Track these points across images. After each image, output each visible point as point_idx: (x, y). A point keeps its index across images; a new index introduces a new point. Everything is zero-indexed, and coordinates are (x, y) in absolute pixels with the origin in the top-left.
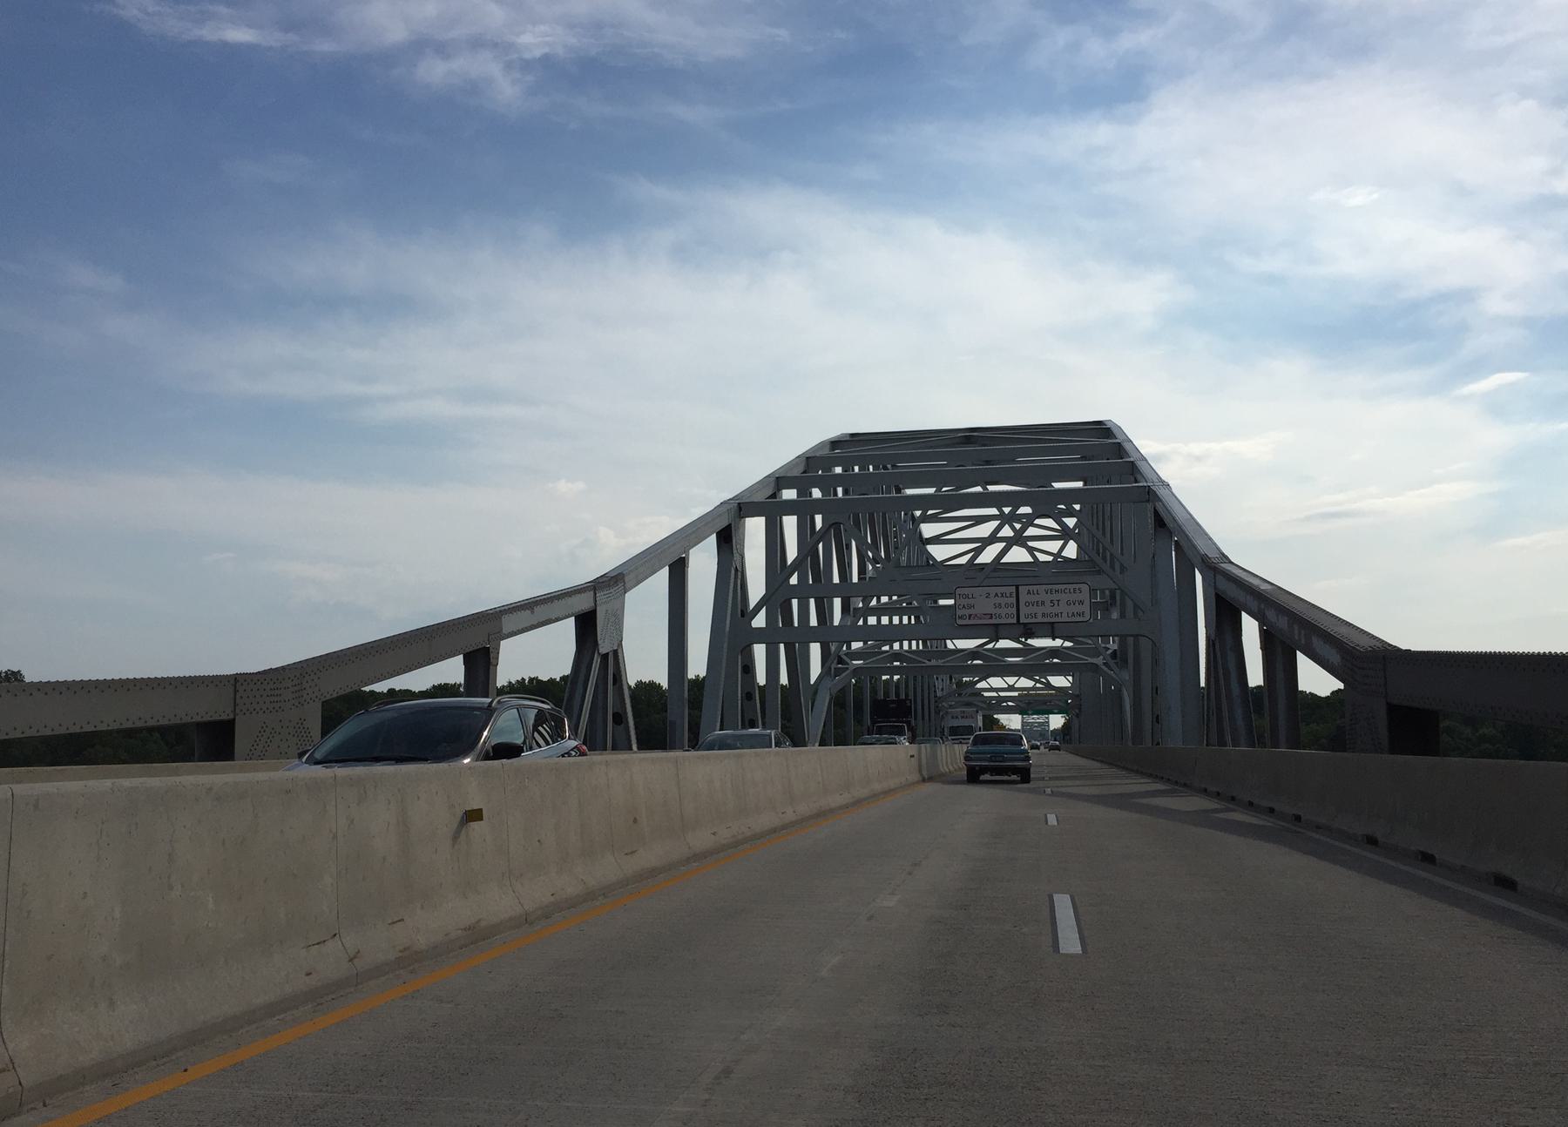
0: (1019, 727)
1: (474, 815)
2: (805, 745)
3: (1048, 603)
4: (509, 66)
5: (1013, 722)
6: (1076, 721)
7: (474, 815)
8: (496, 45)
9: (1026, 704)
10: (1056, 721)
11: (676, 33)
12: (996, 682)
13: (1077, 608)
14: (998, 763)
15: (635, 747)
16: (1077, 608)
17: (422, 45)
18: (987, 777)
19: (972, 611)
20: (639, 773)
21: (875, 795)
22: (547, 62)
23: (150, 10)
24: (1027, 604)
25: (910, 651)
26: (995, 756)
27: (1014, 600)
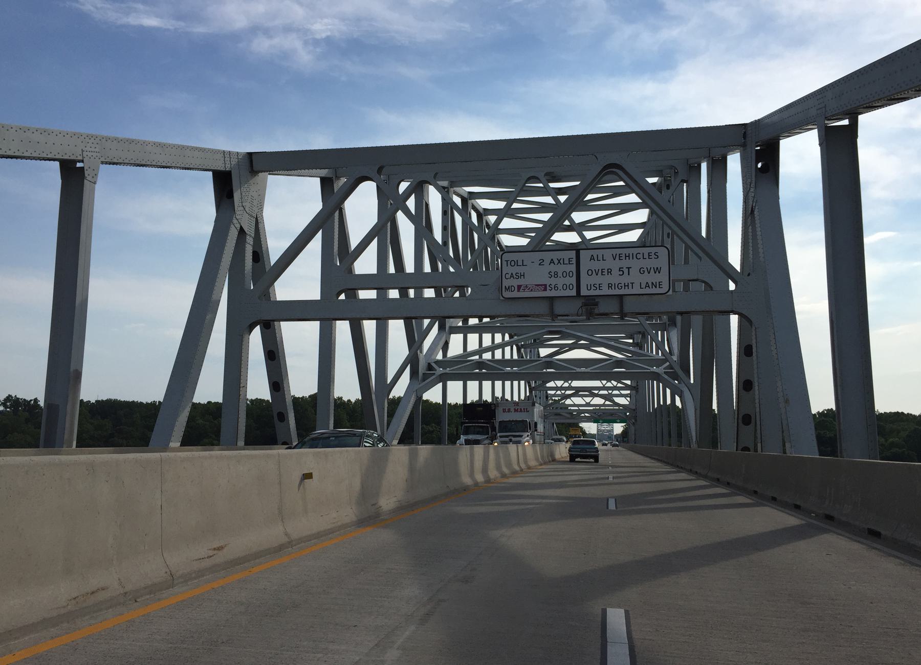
0: (595, 432)
1: (308, 476)
2: (54, 447)
3: (616, 272)
4: (306, 43)
5: (591, 428)
6: (633, 428)
7: (308, 476)
8: (298, 30)
9: (598, 416)
10: (618, 428)
11: (401, 24)
12: (578, 400)
13: (653, 278)
14: (584, 451)
15: (241, 443)
16: (653, 278)
17: (255, 30)
18: (578, 459)
19: (521, 282)
20: (234, 467)
21: (291, 543)
22: (328, 40)
23: (99, 6)
24: (590, 272)
25: (493, 360)
26: (582, 450)
27: (573, 268)
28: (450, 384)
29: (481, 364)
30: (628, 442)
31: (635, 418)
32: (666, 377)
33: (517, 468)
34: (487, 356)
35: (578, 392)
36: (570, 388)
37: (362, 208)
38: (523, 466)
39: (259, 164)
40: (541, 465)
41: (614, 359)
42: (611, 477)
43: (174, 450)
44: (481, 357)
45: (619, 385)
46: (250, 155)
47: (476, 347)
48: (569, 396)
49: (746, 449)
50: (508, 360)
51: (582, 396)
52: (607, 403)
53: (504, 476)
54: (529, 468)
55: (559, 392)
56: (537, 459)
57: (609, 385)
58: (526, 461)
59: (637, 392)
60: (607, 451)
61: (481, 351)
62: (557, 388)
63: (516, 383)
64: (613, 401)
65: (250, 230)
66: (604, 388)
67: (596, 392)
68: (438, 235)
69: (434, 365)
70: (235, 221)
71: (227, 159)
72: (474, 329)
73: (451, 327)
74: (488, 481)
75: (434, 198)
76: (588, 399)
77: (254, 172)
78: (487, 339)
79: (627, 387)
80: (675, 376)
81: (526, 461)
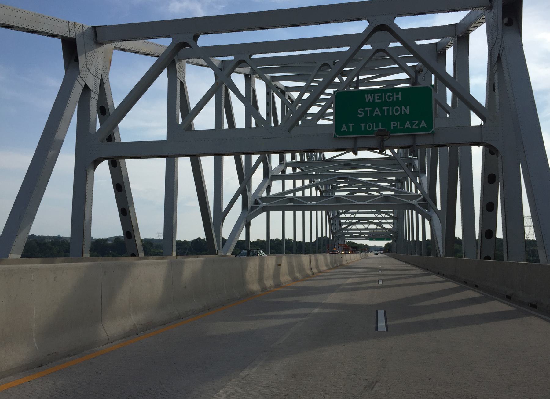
6: (394, 243)
12: (360, 226)
15: (87, 255)
28: (272, 213)
29: (291, 200)
30: (392, 253)
31: (396, 237)
32: (419, 206)
33: (309, 272)
34: (299, 194)
35: (359, 221)
36: (355, 218)
37: (198, 80)
38: (315, 271)
39: (100, 36)
40: (331, 269)
41: (383, 196)
42: (380, 283)
43: (14, 261)
44: (295, 194)
45: (386, 216)
46: (95, 28)
47: (291, 187)
48: (354, 224)
49: (488, 258)
50: (314, 197)
51: (362, 224)
52: (379, 228)
53: (295, 279)
54: (320, 272)
55: (348, 221)
56: (327, 265)
57: (380, 216)
58: (317, 267)
59: (398, 220)
60: (378, 258)
61: (295, 190)
62: (346, 219)
63: (314, 213)
64: (382, 227)
65: (94, 86)
66: (376, 218)
67: (371, 221)
68: (263, 111)
69: (259, 201)
70: (79, 79)
71: (72, 27)
72: (290, 177)
73: (272, 176)
74: (264, 289)
75: (260, 87)
76: (366, 226)
77: (98, 43)
78: (299, 183)
79: (391, 218)
80: (426, 206)
81: (317, 267)
